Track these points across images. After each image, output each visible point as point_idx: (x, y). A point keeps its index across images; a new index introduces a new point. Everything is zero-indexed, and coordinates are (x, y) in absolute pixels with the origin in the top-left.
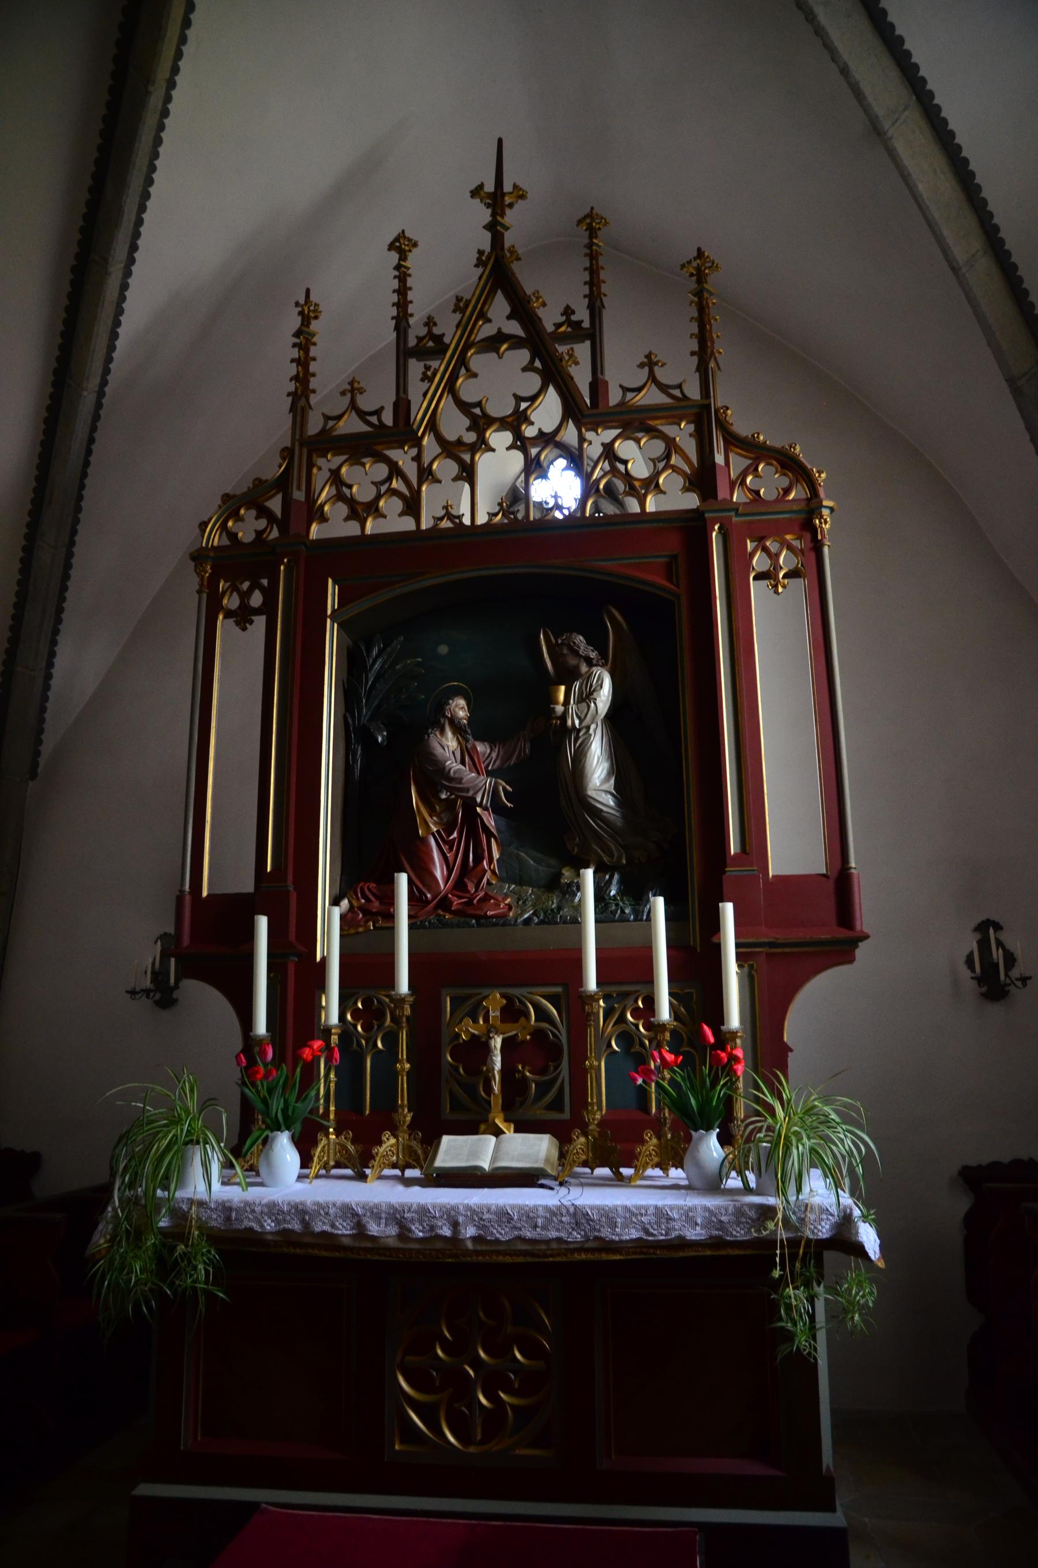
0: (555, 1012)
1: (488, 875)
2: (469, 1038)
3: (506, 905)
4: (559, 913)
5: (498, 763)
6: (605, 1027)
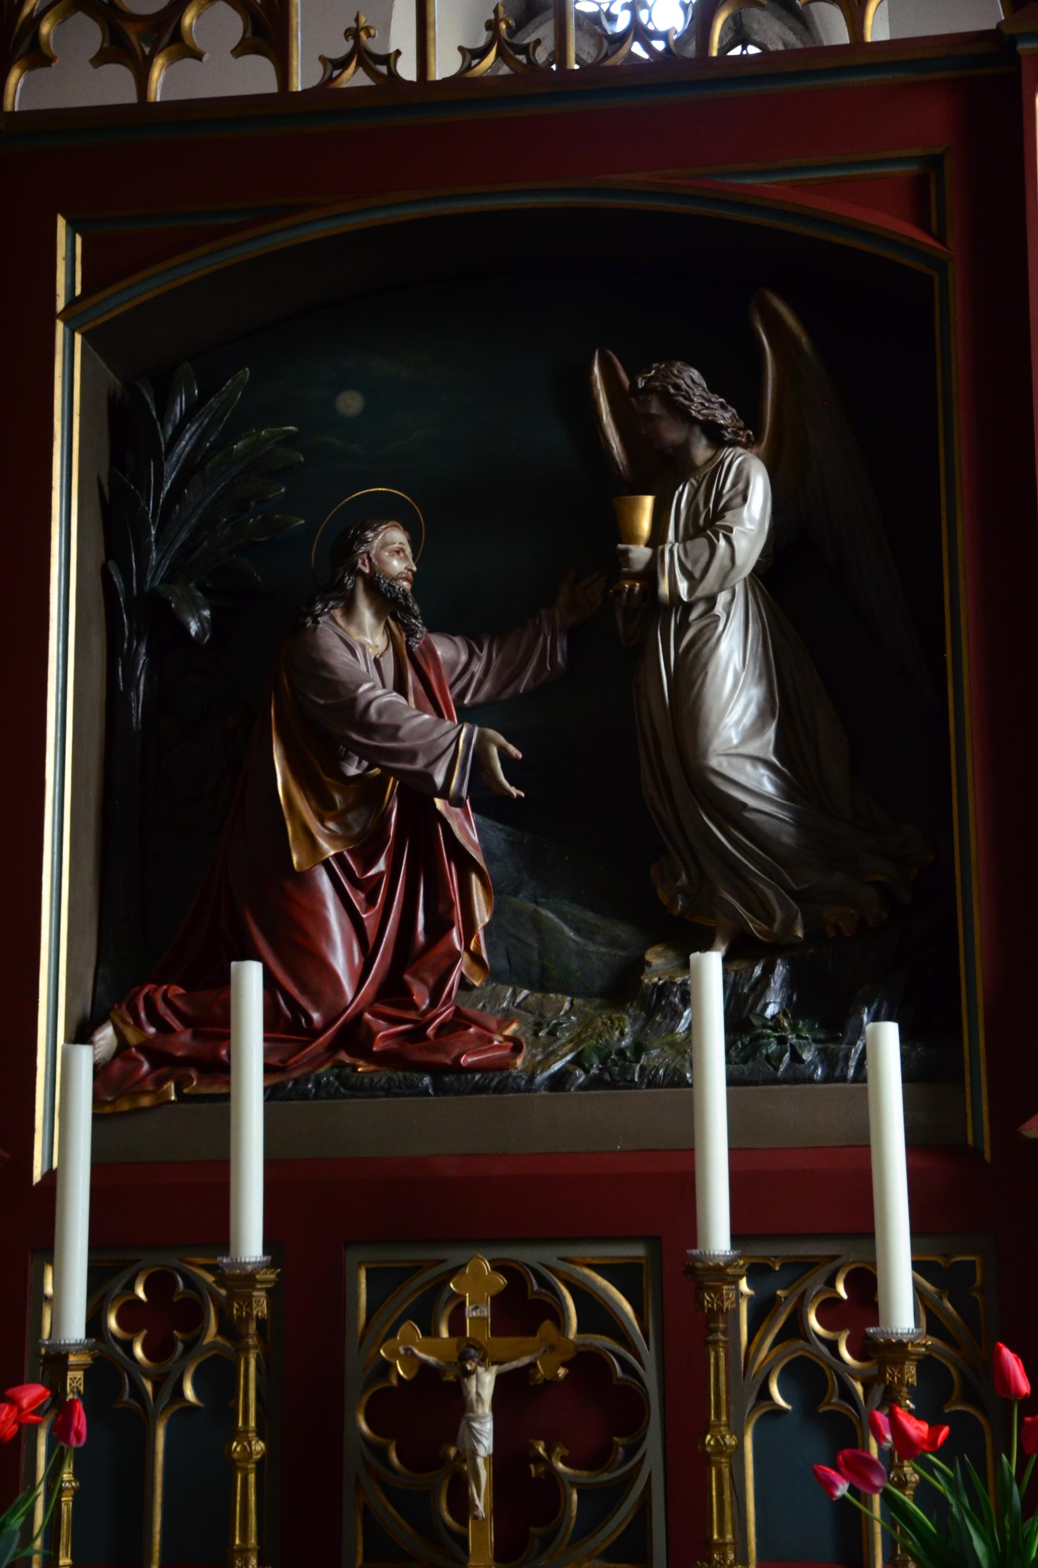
0: (627, 1307)
1: (463, 964)
2: (413, 1374)
3: (507, 1038)
4: (637, 1061)
5: (487, 687)
6: (753, 1347)
